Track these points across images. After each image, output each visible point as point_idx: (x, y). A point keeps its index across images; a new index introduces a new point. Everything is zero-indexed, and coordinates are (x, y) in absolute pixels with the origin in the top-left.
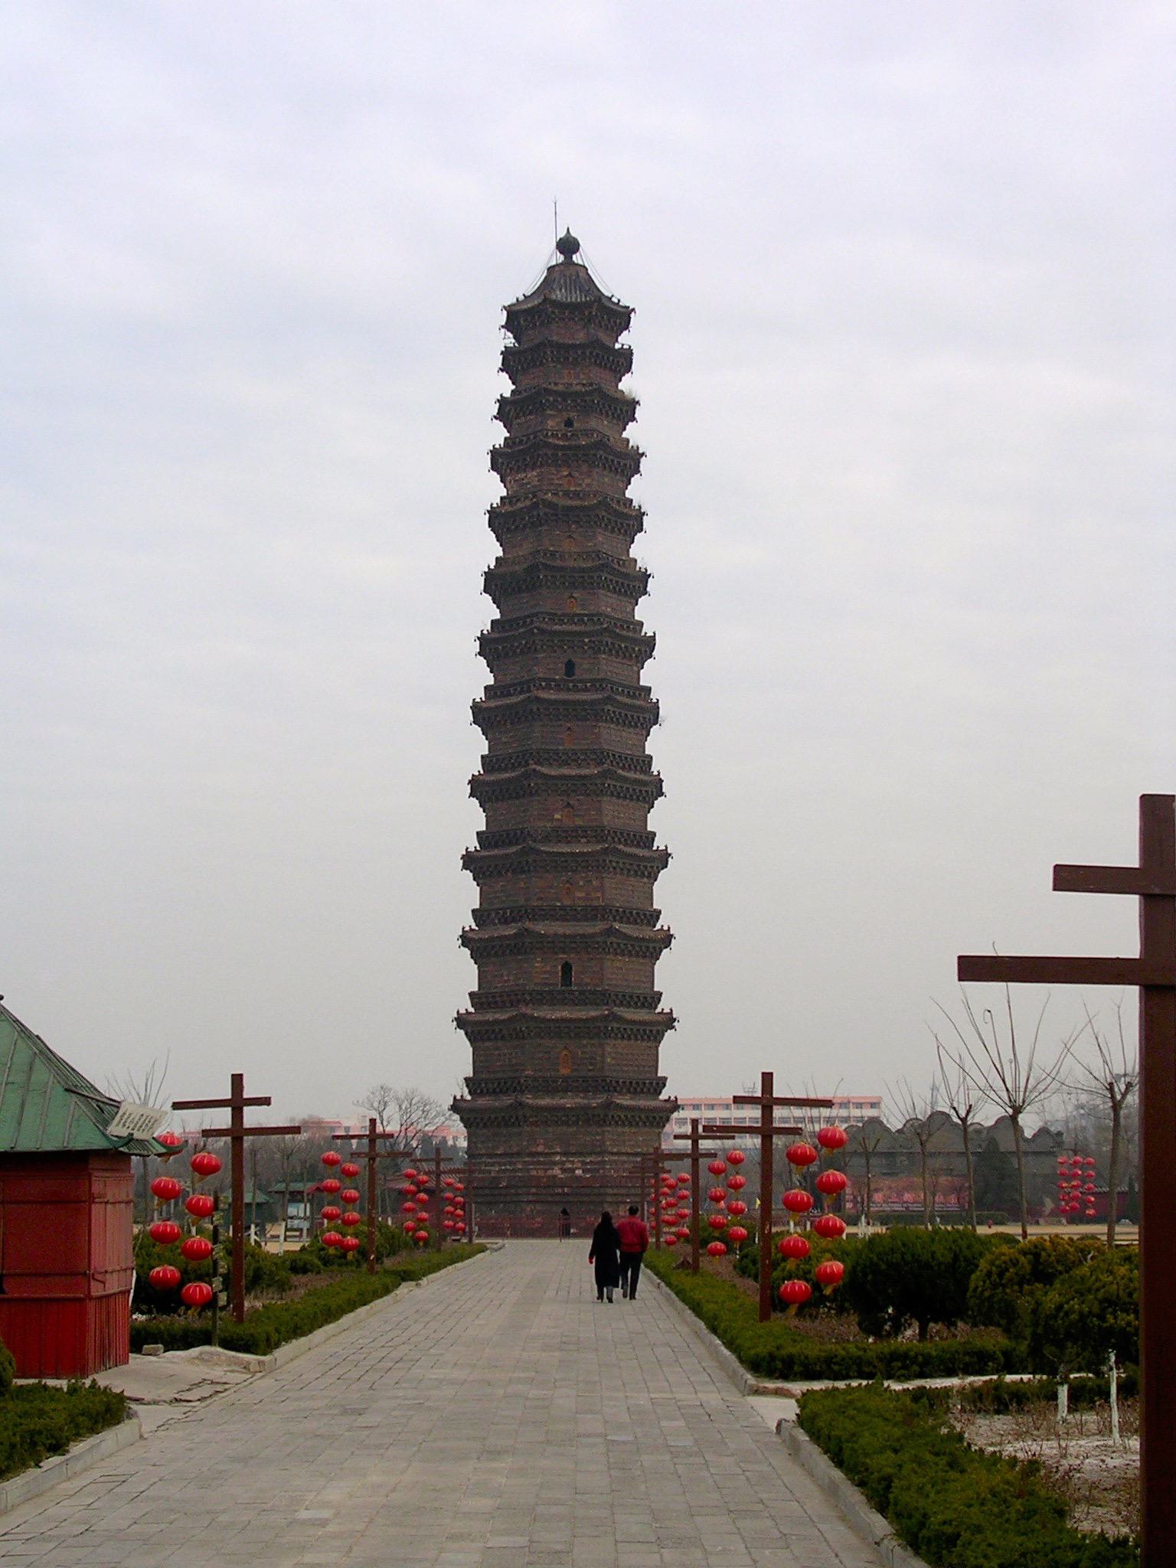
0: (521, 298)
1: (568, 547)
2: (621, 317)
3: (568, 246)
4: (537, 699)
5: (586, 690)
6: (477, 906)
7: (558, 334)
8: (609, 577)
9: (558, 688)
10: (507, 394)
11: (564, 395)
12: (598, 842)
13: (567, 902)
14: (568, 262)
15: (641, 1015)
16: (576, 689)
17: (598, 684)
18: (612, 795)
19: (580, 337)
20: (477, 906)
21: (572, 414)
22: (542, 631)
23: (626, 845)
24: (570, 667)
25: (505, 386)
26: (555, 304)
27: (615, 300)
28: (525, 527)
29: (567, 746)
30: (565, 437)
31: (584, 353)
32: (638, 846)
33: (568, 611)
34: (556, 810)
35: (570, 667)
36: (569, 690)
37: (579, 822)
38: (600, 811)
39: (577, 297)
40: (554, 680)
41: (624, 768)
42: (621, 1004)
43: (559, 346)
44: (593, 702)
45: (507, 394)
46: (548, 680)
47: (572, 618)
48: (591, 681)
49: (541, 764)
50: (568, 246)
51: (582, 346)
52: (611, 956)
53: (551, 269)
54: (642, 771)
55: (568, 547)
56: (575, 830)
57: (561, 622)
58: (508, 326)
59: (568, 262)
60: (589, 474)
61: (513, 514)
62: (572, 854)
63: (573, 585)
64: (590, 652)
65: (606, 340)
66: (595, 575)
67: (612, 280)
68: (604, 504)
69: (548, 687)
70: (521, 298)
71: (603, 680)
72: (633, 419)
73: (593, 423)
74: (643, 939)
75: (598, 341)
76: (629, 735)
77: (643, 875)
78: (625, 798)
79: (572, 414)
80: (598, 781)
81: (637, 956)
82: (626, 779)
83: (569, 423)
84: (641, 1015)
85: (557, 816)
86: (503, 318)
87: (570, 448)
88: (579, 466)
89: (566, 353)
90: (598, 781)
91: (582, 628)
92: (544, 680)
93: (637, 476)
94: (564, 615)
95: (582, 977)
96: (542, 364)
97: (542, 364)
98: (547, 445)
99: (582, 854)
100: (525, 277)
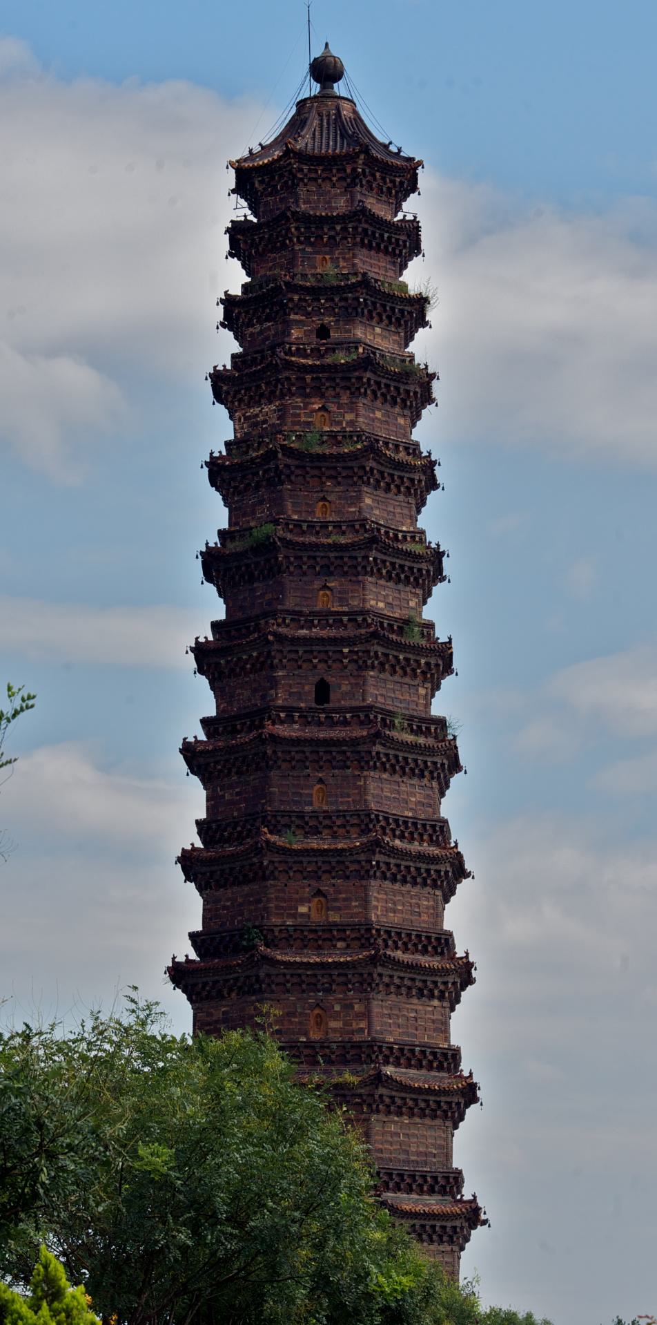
0: (257, 149)
1: (312, 422)
2: (401, 176)
3: (325, 71)
4: (274, 738)
5: (345, 723)
6: (199, 927)
7: (308, 201)
8: (380, 556)
9: (307, 718)
10: (236, 291)
11: (315, 292)
12: (362, 946)
13: (315, 1036)
14: (325, 96)
15: (433, 1203)
16: (332, 724)
17: (363, 715)
18: (384, 877)
19: (341, 205)
20: (199, 927)
21: (327, 319)
22: (280, 638)
23: (406, 950)
24: (323, 691)
25: (234, 278)
26: (301, 156)
27: (393, 149)
28: (257, 487)
29: (316, 806)
30: (316, 353)
31: (345, 229)
32: (425, 952)
33: (319, 607)
34: (302, 901)
35: (323, 691)
36: (320, 724)
37: (335, 917)
38: (365, 902)
39: (332, 146)
40: (299, 709)
41: (402, 837)
42: (398, 1188)
43: (306, 219)
44: (354, 742)
45: (236, 291)
46: (290, 710)
47: (325, 617)
48: (352, 709)
49: (279, 832)
50: (325, 71)
51: (342, 219)
52: (382, 1117)
53: (301, 104)
54: (438, 844)
55: (312, 422)
56: (329, 927)
57: (310, 625)
58: (240, 189)
59: (325, 96)
60: (352, 408)
61: (240, 467)
62: (322, 965)
63: (328, 571)
64: (352, 667)
65: (380, 210)
66: (360, 554)
67: (387, 126)
68: (372, 448)
69: (290, 720)
70: (257, 149)
71: (370, 707)
72: (424, 324)
73: (359, 333)
74: (430, 1091)
75: (364, 211)
76: (424, 897)
77: (432, 996)
78: (404, 881)
79: (327, 319)
80: (362, 857)
81: (423, 1116)
82: (405, 854)
83: (323, 332)
84: (433, 1203)
85: (303, 909)
86: (230, 179)
87: (322, 368)
88: (338, 396)
89: (322, 221)
90: (362, 857)
91: (342, 633)
92: (283, 709)
93: (430, 407)
94: (312, 613)
95: (342, 693)
96: (284, 246)
97: (284, 246)
98: (289, 365)
99: (337, 965)
100: (260, 127)
